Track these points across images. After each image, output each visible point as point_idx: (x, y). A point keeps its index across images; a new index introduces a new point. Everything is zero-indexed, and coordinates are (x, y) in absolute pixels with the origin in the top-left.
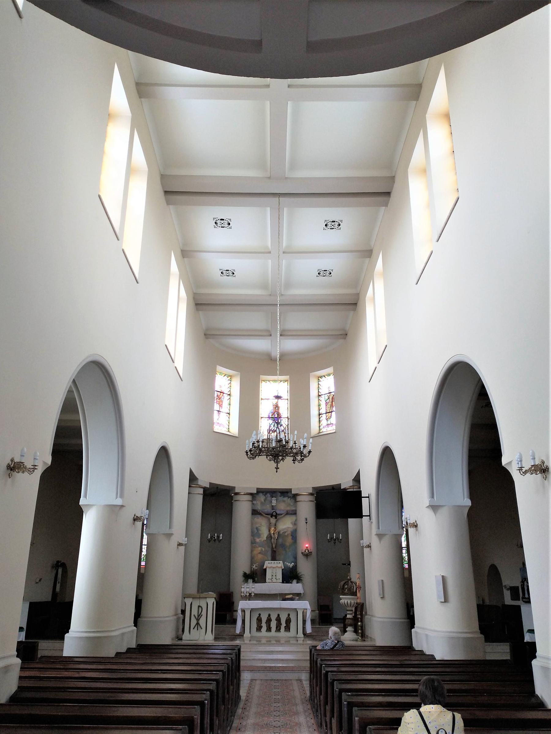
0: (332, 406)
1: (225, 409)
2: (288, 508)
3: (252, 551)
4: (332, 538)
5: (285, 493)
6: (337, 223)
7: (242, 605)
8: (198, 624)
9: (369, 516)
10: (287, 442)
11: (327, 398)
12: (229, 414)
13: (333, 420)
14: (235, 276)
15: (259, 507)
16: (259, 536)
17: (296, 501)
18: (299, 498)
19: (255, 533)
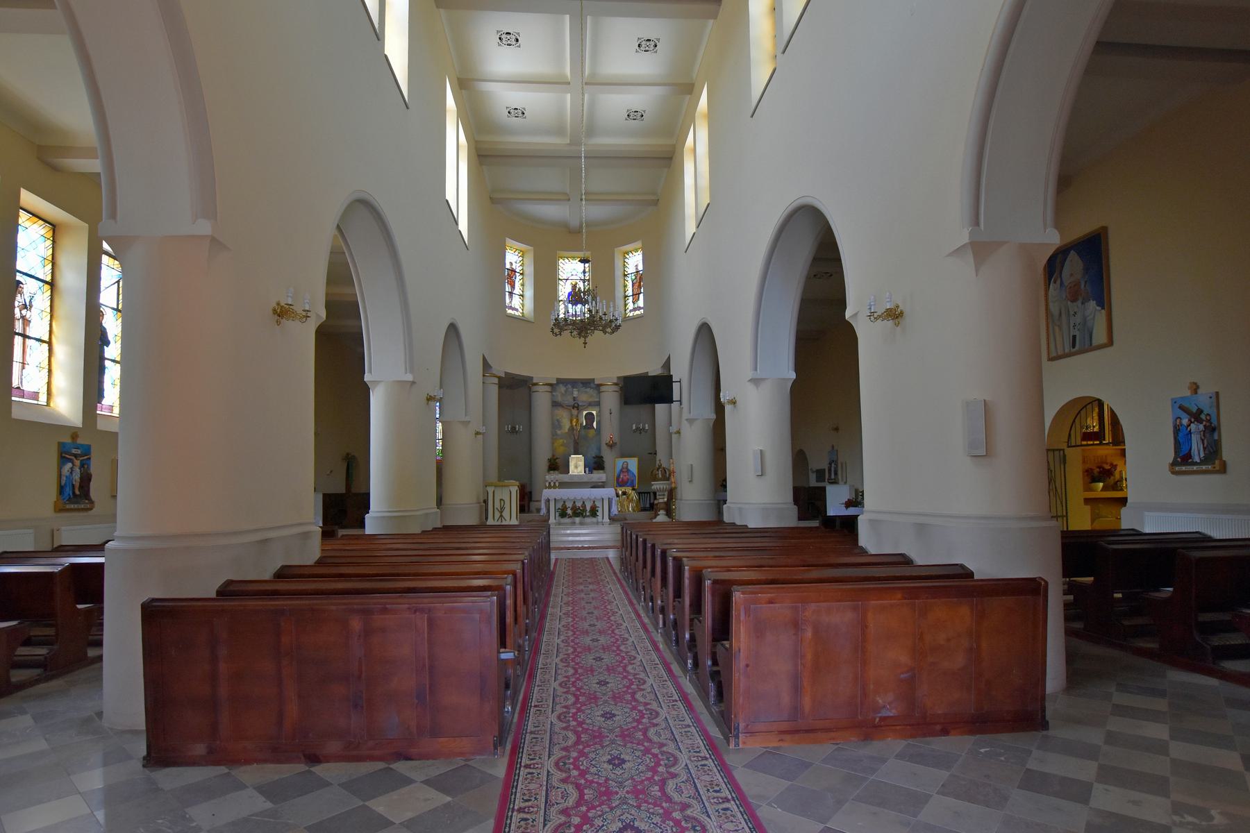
0: (640, 287)
1: (517, 290)
2: (590, 400)
3: (553, 443)
4: (637, 428)
5: (587, 383)
6: (653, 43)
7: (547, 493)
8: (501, 516)
9: (680, 401)
10: (597, 312)
11: (634, 278)
12: (522, 296)
13: (641, 303)
14: (525, 118)
15: (559, 399)
16: (560, 427)
17: (600, 392)
18: (603, 389)
19: (556, 425)
